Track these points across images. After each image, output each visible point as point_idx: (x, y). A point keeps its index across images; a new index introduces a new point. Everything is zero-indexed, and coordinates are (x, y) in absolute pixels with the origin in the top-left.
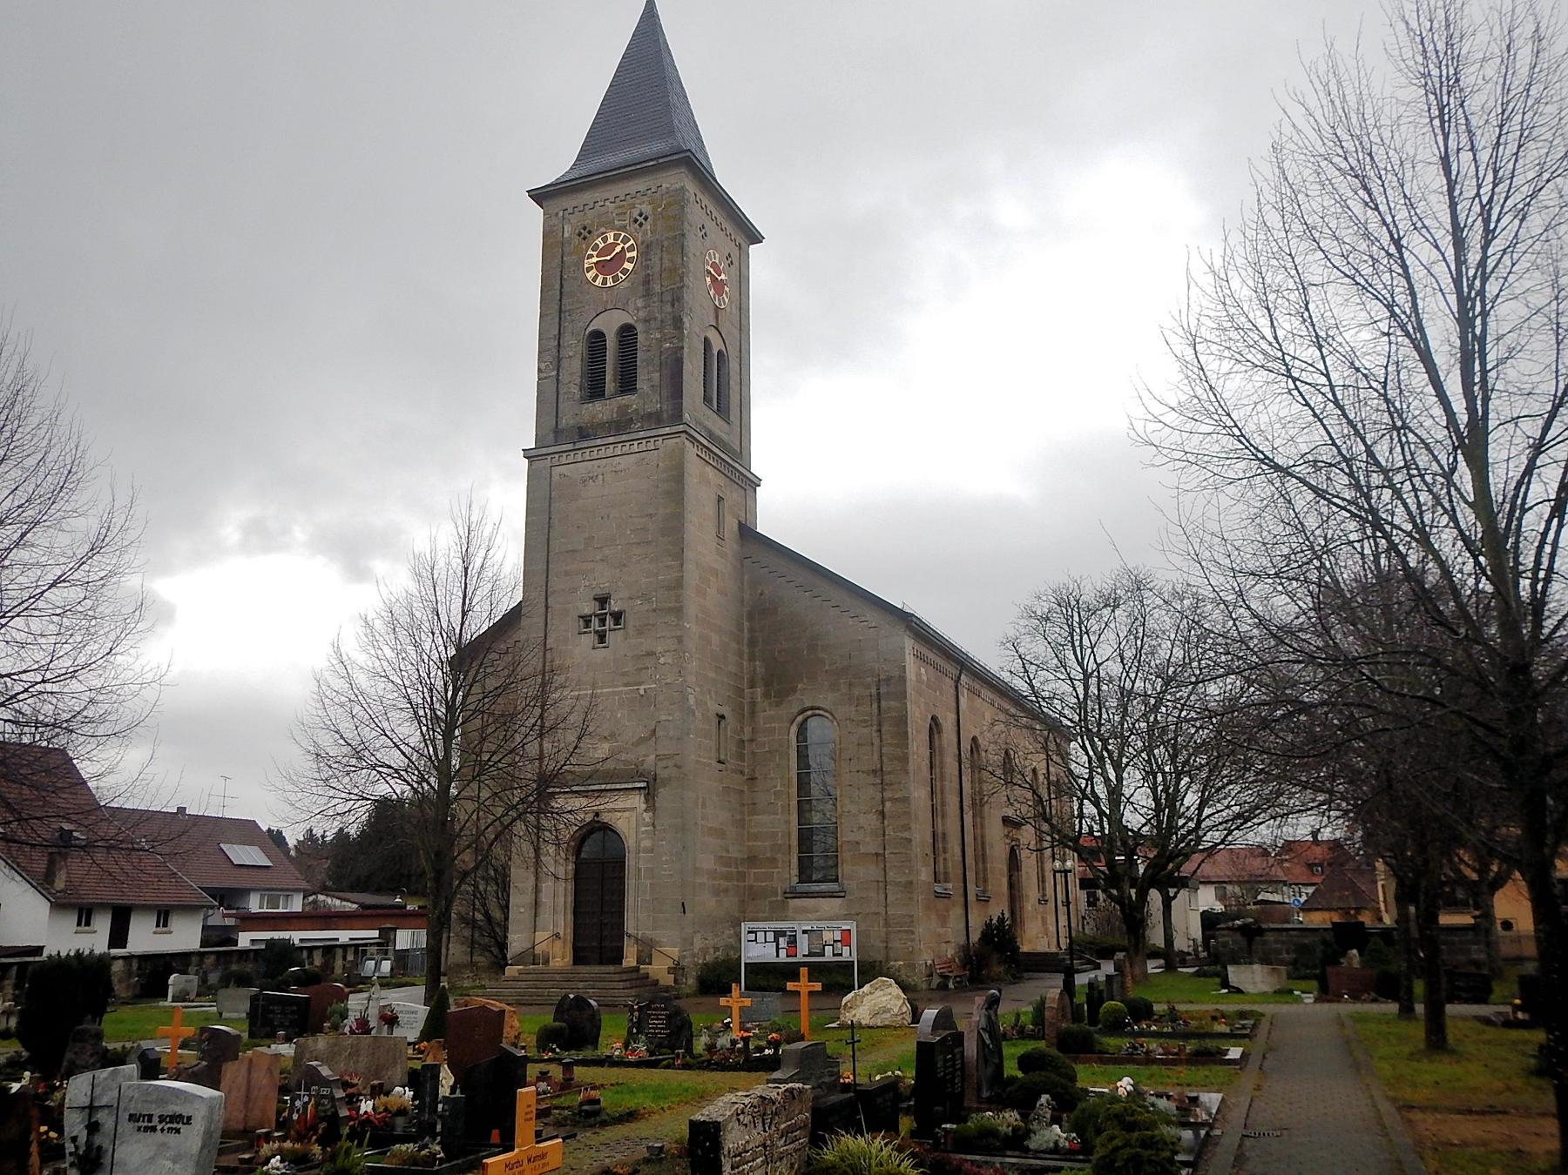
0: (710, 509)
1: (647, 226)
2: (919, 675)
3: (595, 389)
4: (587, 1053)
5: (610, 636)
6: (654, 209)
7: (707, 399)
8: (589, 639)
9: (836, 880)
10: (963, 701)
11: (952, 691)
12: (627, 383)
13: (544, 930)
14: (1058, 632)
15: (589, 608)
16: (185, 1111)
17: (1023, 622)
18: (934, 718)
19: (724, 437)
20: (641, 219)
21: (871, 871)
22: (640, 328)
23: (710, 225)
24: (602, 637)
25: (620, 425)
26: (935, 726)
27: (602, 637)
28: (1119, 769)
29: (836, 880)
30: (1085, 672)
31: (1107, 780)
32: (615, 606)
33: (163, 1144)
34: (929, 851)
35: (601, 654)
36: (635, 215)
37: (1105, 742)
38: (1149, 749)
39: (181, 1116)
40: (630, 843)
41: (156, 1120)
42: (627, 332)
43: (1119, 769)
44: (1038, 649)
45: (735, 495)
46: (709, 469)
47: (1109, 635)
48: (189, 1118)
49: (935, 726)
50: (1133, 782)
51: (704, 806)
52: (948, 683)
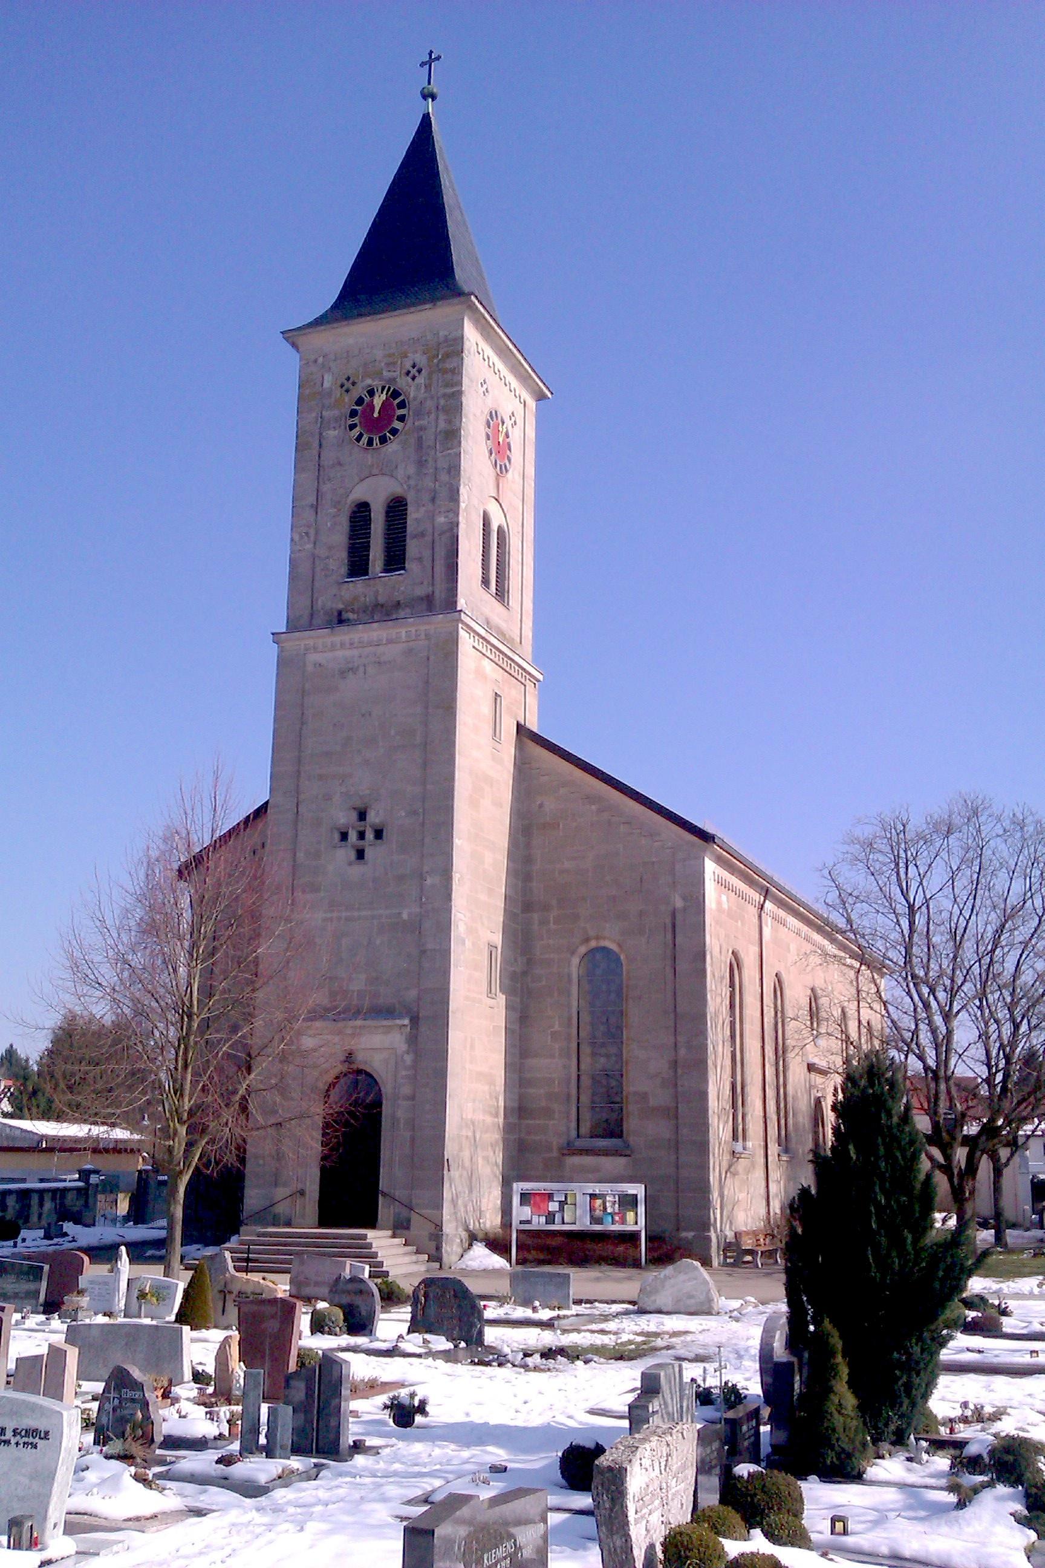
0: (486, 709)
1: (421, 380)
2: (719, 903)
3: (358, 566)
4: (361, 1341)
5: (369, 853)
6: (430, 359)
7: (485, 582)
8: (344, 854)
9: (620, 1136)
10: (767, 932)
11: (756, 921)
12: (395, 560)
13: (285, 1185)
14: (882, 859)
15: (345, 818)
16: (41, 1425)
17: (845, 848)
18: (734, 953)
19: (503, 625)
20: (414, 371)
21: (660, 1129)
22: (410, 498)
23: (493, 380)
24: (360, 854)
25: (385, 611)
26: (735, 965)
27: (360, 854)
28: (947, 1017)
29: (620, 1136)
30: (911, 907)
31: (934, 1031)
32: (373, 818)
33: (18, 1459)
34: (728, 1106)
35: (357, 871)
36: (408, 365)
37: (932, 991)
38: (982, 995)
39: (36, 1430)
40: (387, 1089)
41: (9, 1435)
42: (397, 509)
43: (947, 1017)
44: (856, 879)
45: (514, 692)
46: (486, 662)
47: (939, 866)
48: (47, 1433)
49: (735, 965)
50: (965, 1032)
51: (472, 1047)
52: (753, 911)
